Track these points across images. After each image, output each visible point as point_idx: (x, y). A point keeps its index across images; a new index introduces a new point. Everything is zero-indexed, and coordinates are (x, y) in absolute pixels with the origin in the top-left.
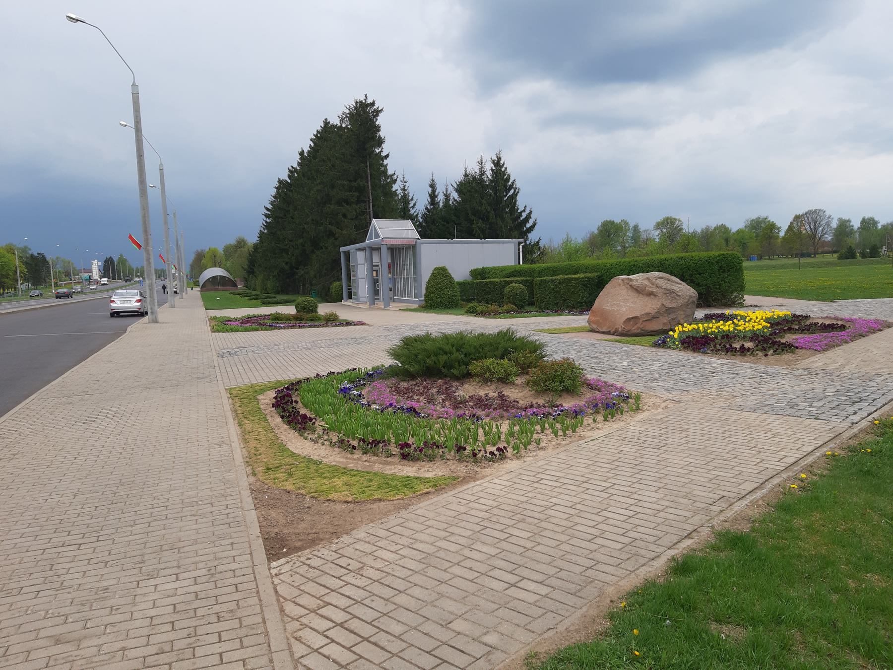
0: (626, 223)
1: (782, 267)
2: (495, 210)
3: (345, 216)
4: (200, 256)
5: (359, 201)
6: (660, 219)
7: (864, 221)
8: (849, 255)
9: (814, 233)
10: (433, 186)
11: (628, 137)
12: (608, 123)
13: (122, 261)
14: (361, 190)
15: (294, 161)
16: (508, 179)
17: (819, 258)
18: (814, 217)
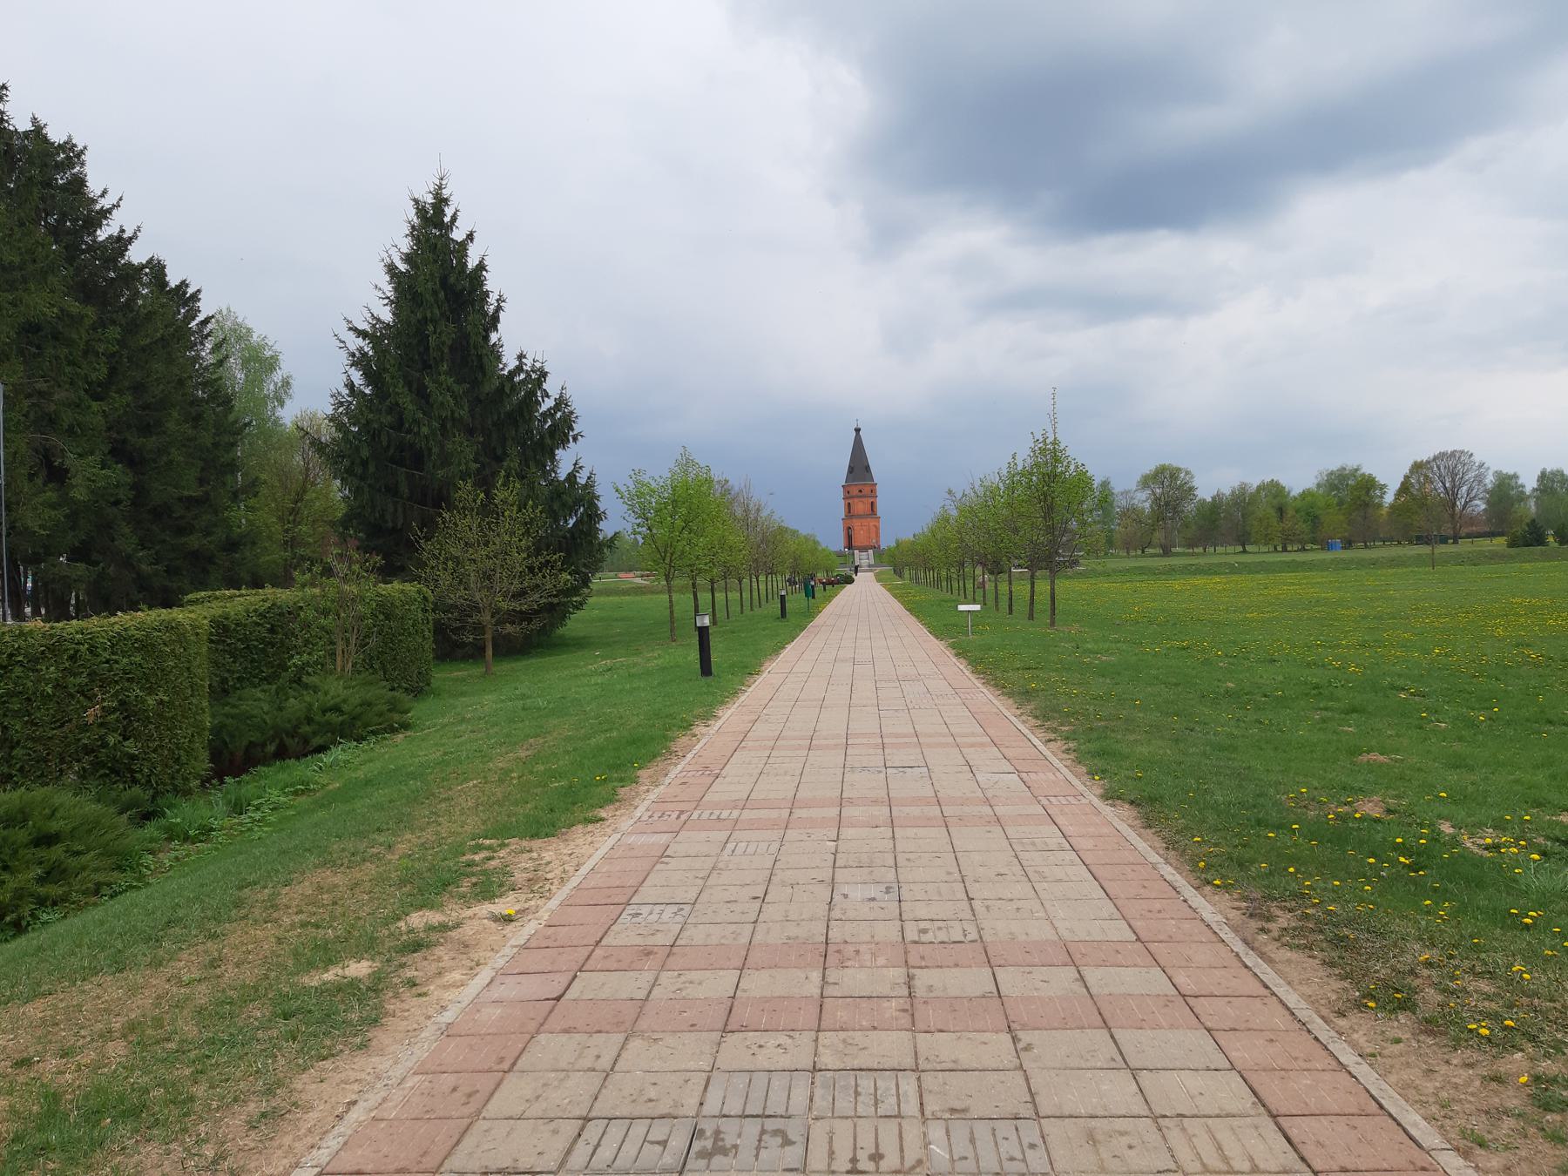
1: (1393, 563)
6: (1149, 467)
7: (1543, 476)
8: (1532, 537)
9: (1453, 494)
11: (1146, 330)
12: (1107, 306)
17: (1465, 546)
18: (1451, 464)
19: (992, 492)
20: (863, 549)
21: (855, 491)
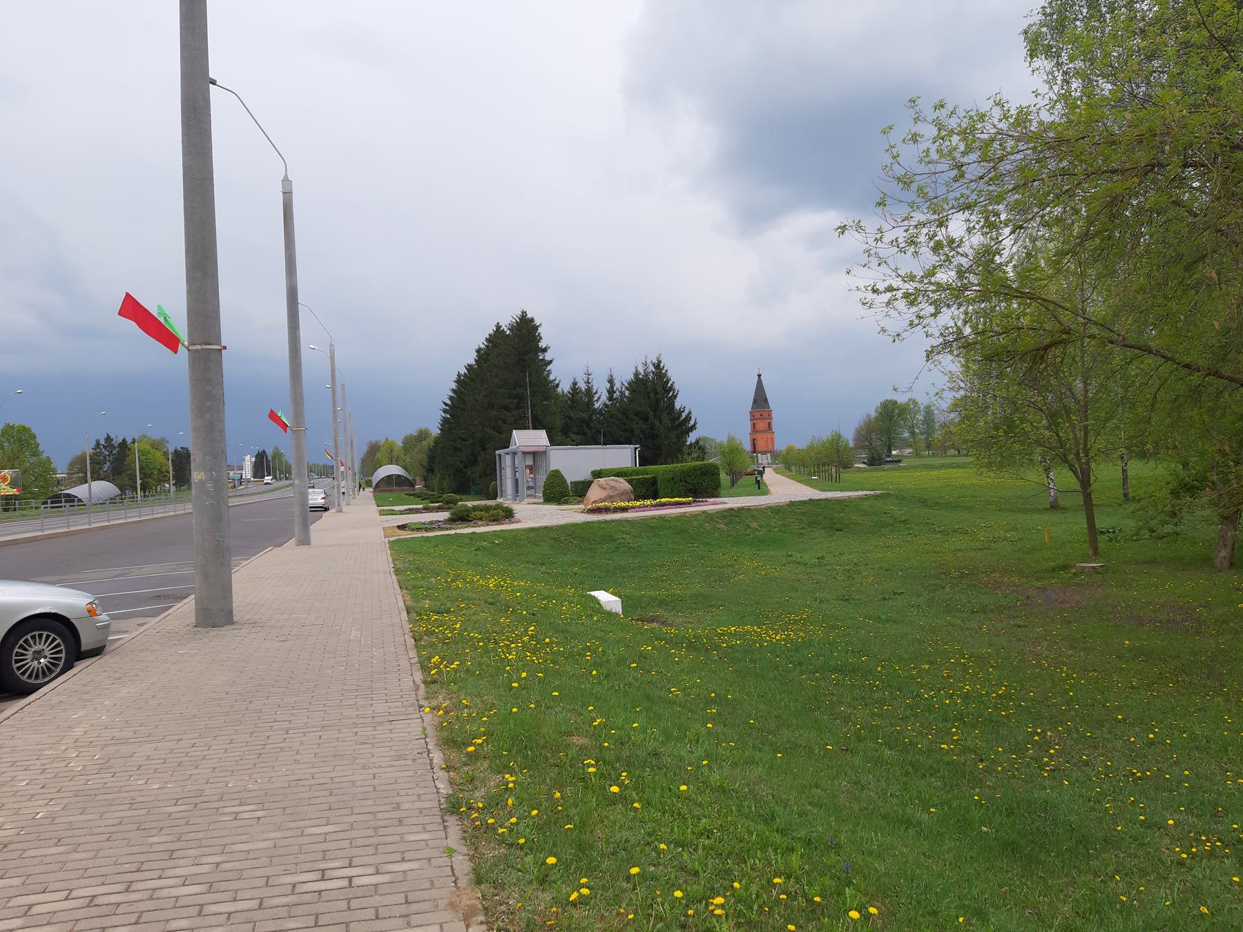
0: (915, 403)
2: (655, 411)
3: (504, 422)
4: (374, 449)
5: (518, 407)
10: (611, 381)
13: (277, 455)
14: (520, 398)
15: (471, 359)
16: (667, 382)
19: (861, 428)
20: (764, 453)
21: (757, 415)
